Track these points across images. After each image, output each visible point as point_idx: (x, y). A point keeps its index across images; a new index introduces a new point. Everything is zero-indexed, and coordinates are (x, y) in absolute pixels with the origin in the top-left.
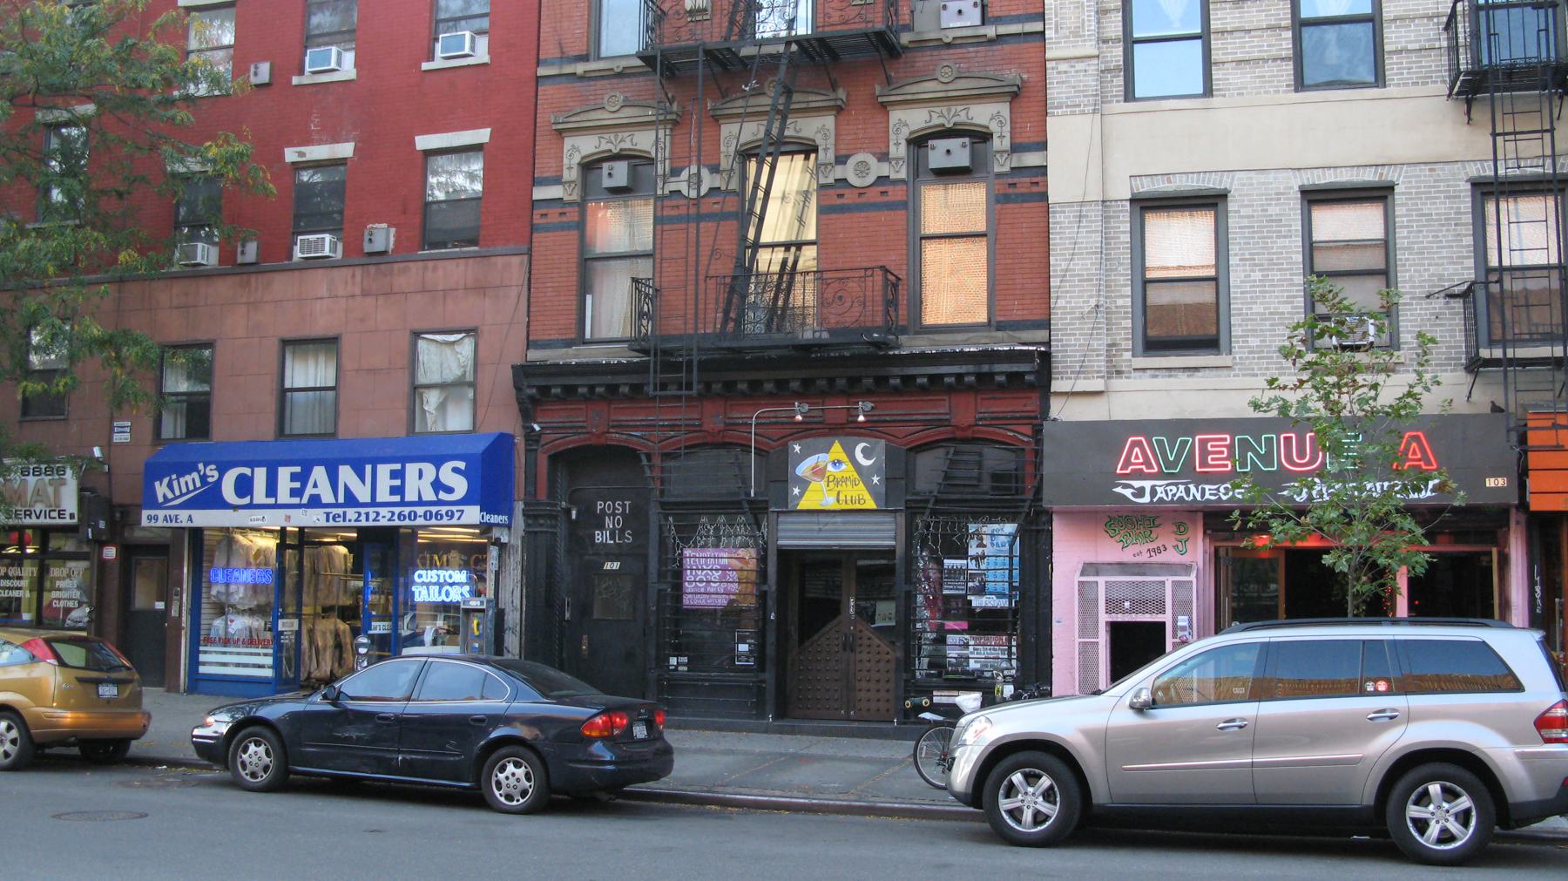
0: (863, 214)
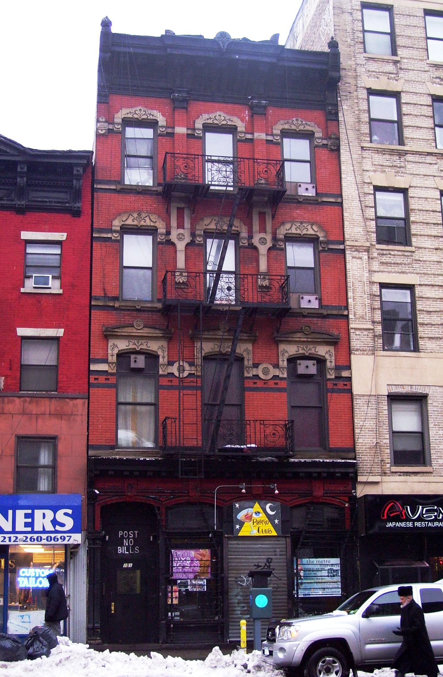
0: (266, 393)
